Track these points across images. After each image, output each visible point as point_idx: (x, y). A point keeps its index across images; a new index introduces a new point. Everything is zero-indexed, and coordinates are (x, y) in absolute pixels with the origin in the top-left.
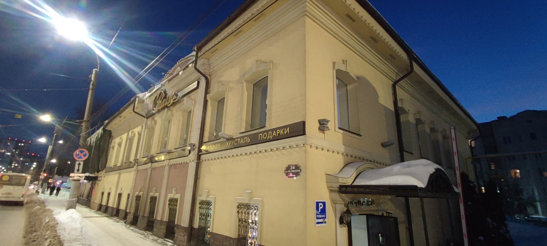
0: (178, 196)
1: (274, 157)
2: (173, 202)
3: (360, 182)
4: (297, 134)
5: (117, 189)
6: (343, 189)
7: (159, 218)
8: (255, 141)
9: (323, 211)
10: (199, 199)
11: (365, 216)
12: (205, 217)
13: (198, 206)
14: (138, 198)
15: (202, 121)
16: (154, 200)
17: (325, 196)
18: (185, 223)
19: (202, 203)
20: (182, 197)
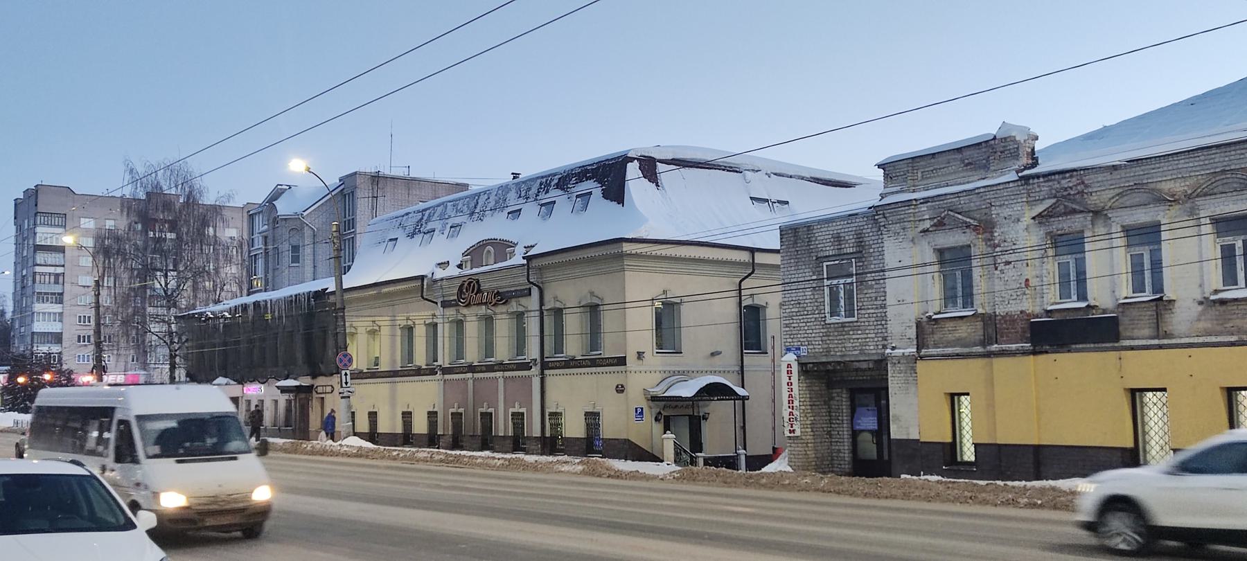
0: (523, 410)
1: (609, 378)
2: (518, 417)
3: (673, 393)
4: (103, 491)
5: (393, 405)
6: (654, 399)
7: (501, 434)
8: (594, 363)
9: (642, 413)
10: (547, 411)
11: (949, 440)
12: (556, 426)
13: (547, 417)
14: (456, 416)
15: (708, 157)
16: (487, 417)
17: (643, 404)
18: (537, 432)
19: (551, 414)
20: (530, 411)
